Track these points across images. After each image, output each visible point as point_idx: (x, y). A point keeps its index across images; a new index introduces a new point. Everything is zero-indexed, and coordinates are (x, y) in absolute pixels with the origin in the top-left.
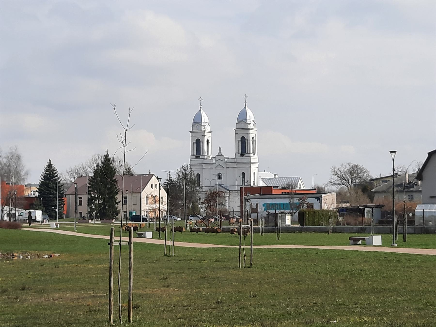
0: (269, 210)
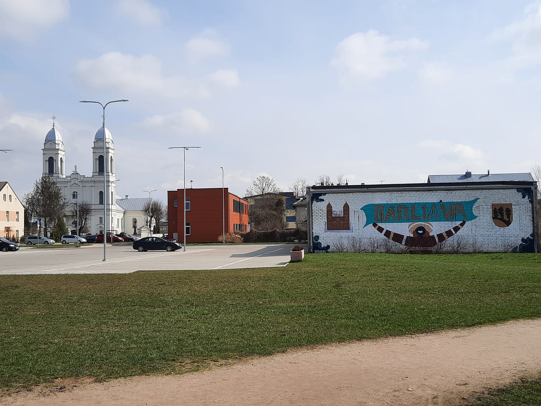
0: (382, 221)
